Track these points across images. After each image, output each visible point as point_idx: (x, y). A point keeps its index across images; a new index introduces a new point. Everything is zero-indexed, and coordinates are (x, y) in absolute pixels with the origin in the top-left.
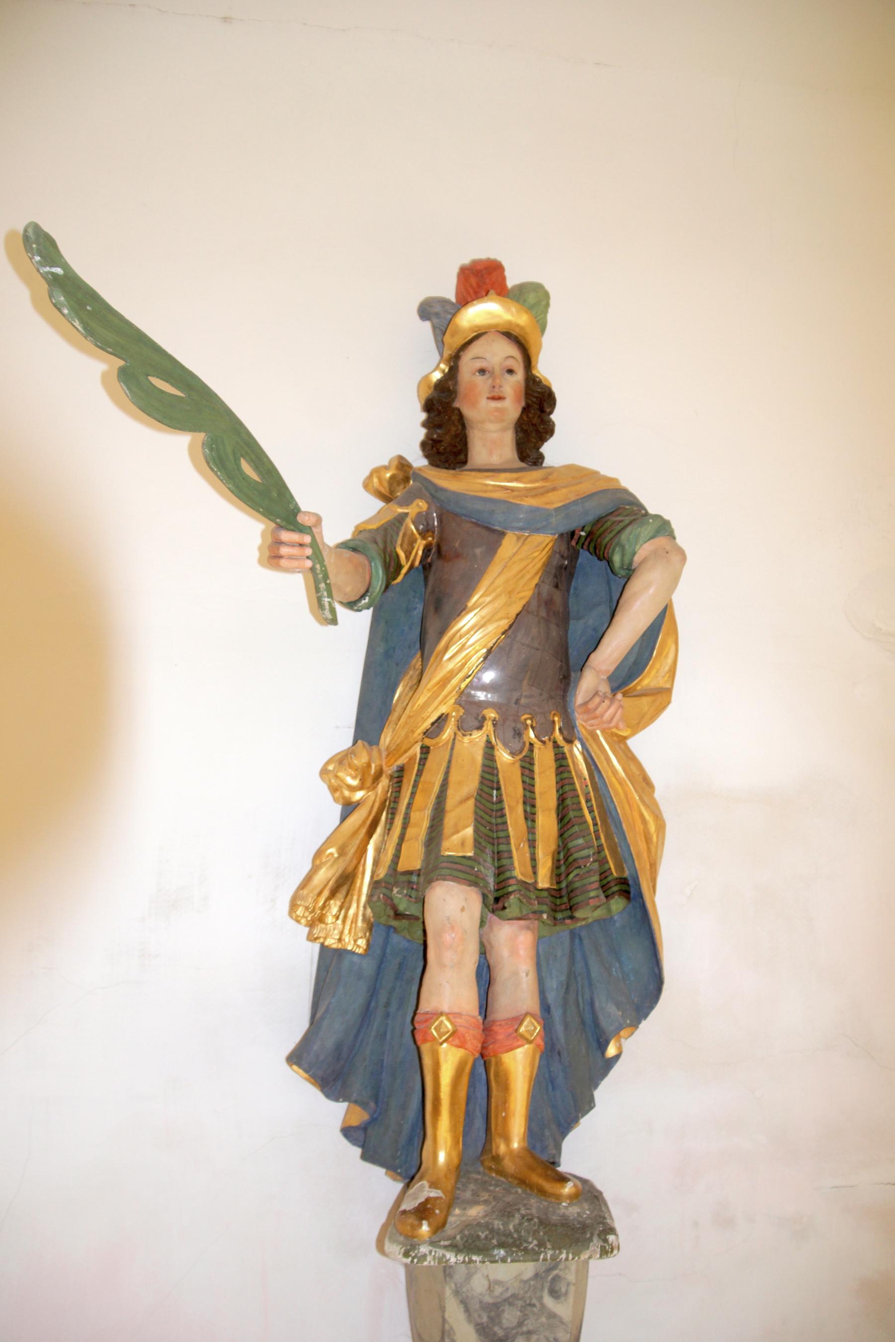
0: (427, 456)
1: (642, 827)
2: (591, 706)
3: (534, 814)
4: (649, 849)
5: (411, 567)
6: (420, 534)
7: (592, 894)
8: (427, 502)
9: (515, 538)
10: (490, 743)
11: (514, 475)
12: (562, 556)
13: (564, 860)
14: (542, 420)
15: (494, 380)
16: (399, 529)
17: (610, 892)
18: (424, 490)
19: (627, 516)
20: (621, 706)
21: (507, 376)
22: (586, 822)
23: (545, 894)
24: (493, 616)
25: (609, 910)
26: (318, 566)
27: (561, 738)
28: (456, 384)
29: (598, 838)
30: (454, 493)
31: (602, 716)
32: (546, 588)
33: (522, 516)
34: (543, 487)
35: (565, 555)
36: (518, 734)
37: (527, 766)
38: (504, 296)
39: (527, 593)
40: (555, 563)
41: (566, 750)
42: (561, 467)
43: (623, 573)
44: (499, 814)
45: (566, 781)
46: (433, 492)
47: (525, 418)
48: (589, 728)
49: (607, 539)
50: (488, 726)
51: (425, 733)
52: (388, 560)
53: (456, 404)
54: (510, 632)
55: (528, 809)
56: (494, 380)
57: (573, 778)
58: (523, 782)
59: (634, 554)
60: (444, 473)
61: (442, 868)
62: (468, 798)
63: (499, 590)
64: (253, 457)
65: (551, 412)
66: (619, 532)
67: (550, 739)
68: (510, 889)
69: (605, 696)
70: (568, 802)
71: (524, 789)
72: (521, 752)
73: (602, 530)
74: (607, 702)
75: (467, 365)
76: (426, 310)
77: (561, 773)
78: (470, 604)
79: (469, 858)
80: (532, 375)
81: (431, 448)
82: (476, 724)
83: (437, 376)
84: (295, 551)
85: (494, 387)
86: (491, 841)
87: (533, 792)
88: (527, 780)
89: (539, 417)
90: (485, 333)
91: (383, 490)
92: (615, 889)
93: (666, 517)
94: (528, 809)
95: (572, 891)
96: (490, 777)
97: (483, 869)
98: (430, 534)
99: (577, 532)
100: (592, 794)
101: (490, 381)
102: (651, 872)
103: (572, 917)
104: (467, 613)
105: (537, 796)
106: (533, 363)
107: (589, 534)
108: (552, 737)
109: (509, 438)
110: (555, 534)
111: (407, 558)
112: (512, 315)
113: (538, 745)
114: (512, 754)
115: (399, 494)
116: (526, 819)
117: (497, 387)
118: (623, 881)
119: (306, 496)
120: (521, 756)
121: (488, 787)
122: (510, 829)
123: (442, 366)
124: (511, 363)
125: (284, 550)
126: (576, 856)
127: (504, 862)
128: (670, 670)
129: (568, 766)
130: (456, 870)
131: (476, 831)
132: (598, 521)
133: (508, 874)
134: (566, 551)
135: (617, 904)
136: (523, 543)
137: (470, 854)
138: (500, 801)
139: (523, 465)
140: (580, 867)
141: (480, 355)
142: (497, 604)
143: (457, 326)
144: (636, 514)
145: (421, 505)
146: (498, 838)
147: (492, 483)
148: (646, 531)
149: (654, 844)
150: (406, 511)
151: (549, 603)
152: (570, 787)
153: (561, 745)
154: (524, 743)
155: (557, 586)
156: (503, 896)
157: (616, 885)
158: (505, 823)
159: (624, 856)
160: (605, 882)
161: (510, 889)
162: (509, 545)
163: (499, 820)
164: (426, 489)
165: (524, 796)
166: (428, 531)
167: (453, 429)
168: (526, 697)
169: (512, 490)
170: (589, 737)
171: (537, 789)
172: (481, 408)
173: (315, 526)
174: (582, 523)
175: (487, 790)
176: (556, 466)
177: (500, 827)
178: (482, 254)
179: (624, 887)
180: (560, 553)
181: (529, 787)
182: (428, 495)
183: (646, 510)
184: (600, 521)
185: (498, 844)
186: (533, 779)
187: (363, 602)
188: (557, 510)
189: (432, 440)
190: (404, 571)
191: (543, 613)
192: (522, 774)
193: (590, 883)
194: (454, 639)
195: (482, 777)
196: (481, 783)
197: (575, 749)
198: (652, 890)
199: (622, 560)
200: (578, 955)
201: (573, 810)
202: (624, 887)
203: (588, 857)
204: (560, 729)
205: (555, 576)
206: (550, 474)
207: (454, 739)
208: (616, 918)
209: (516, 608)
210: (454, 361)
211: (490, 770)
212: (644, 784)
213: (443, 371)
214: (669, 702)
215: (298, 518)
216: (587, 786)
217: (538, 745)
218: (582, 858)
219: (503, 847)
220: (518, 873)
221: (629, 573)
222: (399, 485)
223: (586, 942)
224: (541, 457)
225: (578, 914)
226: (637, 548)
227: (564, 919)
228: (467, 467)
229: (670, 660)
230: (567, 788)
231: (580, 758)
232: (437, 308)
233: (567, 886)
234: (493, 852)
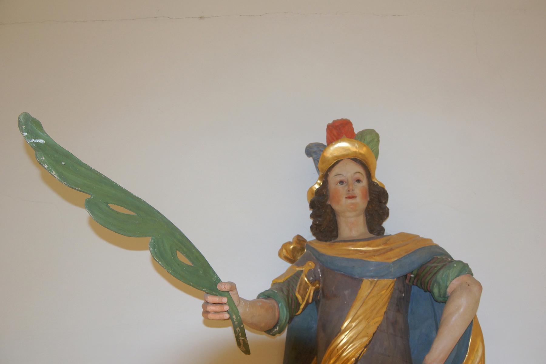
0: (314, 234)
5: (307, 304)
6: (311, 283)
9: (369, 282)
11: (366, 243)
12: (400, 291)
16: (297, 281)
19: (439, 262)
21: (357, 184)
24: (358, 336)
26: (234, 317)
28: (327, 190)
33: (372, 269)
34: (384, 249)
38: (351, 138)
39: (379, 319)
42: (396, 235)
47: (370, 207)
52: (290, 301)
54: (370, 346)
59: (447, 287)
60: (324, 244)
63: (360, 318)
64: (185, 250)
65: (386, 202)
66: (436, 273)
75: (333, 178)
80: (372, 181)
81: (315, 229)
83: (317, 187)
84: (217, 308)
85: (349, 191)
90: (342, 160)
91: (289, 257)
93: (465, 261)
98: (317, 282)
99: (408, 275)
101: (346, 188)
106: (372, 175)
107: (417, 276)
109: (361, 220)
111: (303, 299)
112: (356, 148)
115: (299, 258)
117: (351, 191)
119: (224, 273)
123: (319, 181)
124: (358, 176)
125: (211, 308)
128: (480, 360)
136: (374, 286)
139: (372, 235)
142: (360, 327)
143: (324, 157)
144: (446, 261)
145: (311, 265)
147: (353, 249)
150: (302, 269)
151: (394, 323)
155: (398, 311)
162: (366, 288)
166: (316, 280)
172: (345, 202)
173: (231, 290)
176: (393, 234)
178: (339, 117)
183: (451, 257)
184: (422, 267)
187: (275, 330)
188: (394, 263)
189: (316, 225)
190: (302, 307)
199: (439, 292)
206: (388, 240)
209: (372, 329)
210: (325, 178)
213: (320, 184)
215: (218, 287)
221: (444, 300)
222: (298, 252)
224: (383, 229)
226: (448, 283)
228: (338, 239)
229: (480, 353)
232: (315, 149)
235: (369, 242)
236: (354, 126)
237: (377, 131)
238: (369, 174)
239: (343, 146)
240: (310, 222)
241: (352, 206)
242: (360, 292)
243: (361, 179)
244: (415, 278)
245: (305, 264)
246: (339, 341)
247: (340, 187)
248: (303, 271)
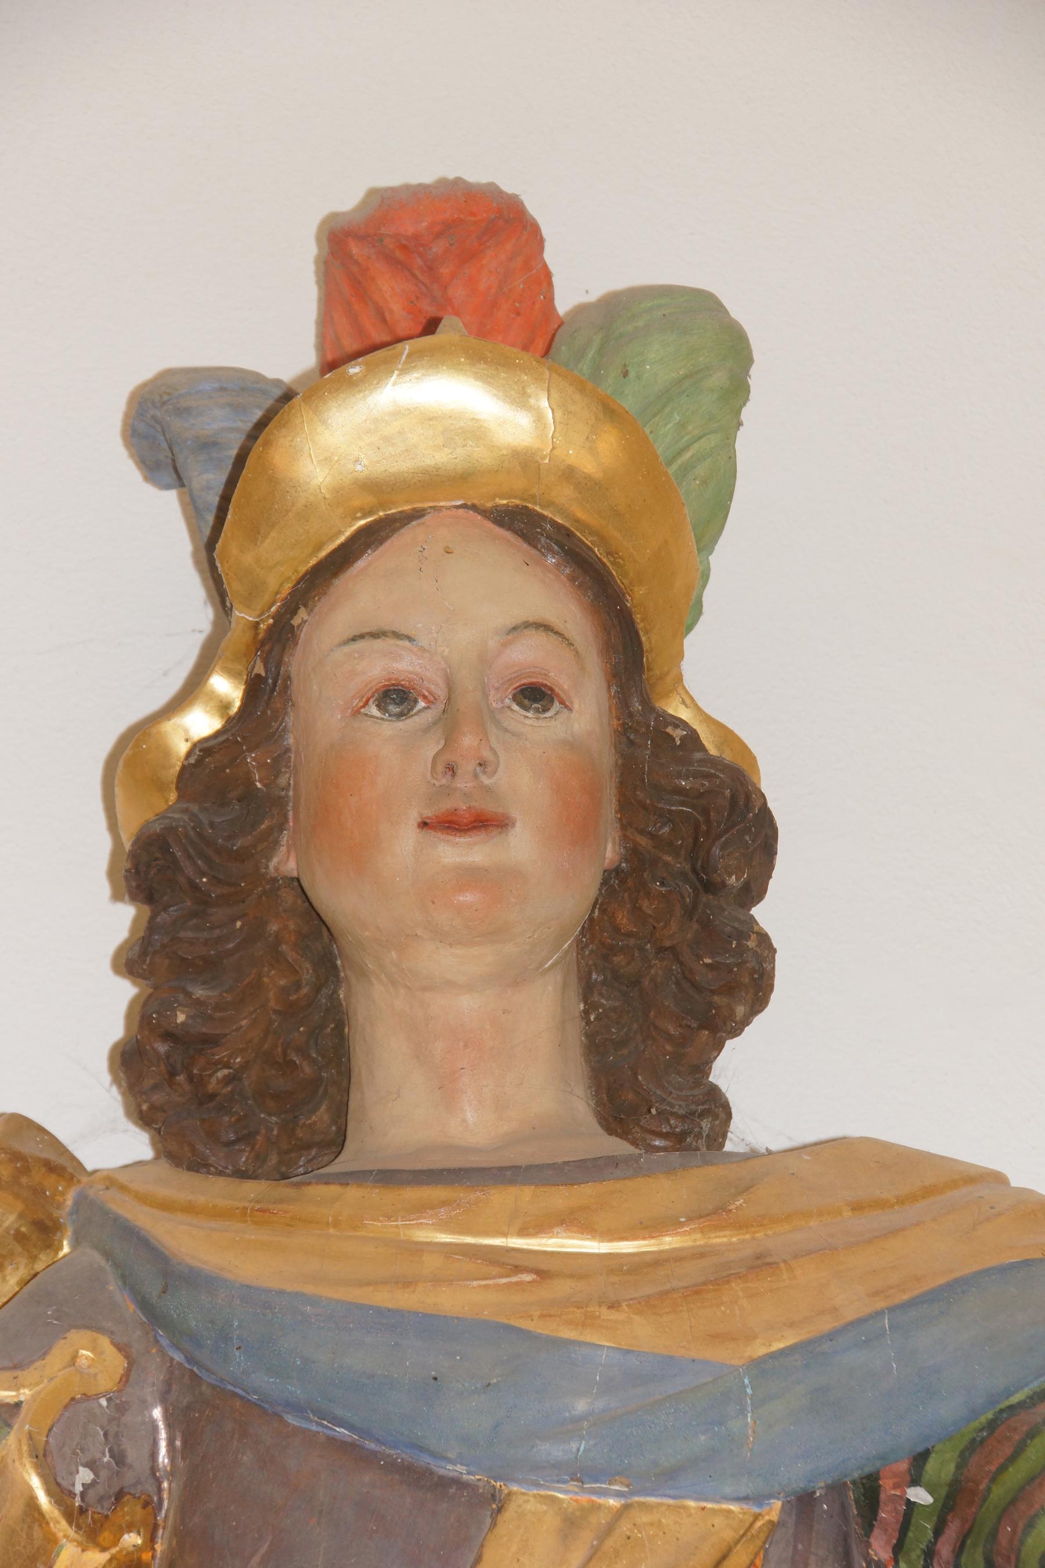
6: (73, 1515)
8: (121, 1348)
9: (552, 1521)
11: (560, 1198)
14: (706, 925)
15: (450, 739)
18: (112, 1285)
21: (525, 721)
28: (280, 761)
30: (249, 1293)
33: (581, 1406)
34: (700, 1254)
46: (152, 1289)
47: (623, 919)
53: (284, 862)
56: (450, 739)
65: (754, 891)
73: (1016, 1474)
75: (333, 666)
76: (161, 429)
81: (157, 1068)
85: (451, 769)
89: (690, 913)
90: (417, 514)
98: (132, 1510)
99: (887, 1488)
101: (431, 748)
107: (955, 1497)
110: (759, 1499)
117: (467, 767)
124: (530, 655)
132: (992, 1425)
141: (386, 620)
164: (126, 1279)
167: (275, 981)
169: (544, 1269)
174: (906, 1435)
182: (131, 1307)
210: (268, 652)
213: (223, 706)
224: (716, 1108)
228: (338, 1166)
235: (586, 1192)
236: (551, 256)
237: (736, 311)
238: (631, 646)
239: (445, 409)
240: (110, 1005)
241: (468, 898)
243: (560, 679)
247: (384, 732)
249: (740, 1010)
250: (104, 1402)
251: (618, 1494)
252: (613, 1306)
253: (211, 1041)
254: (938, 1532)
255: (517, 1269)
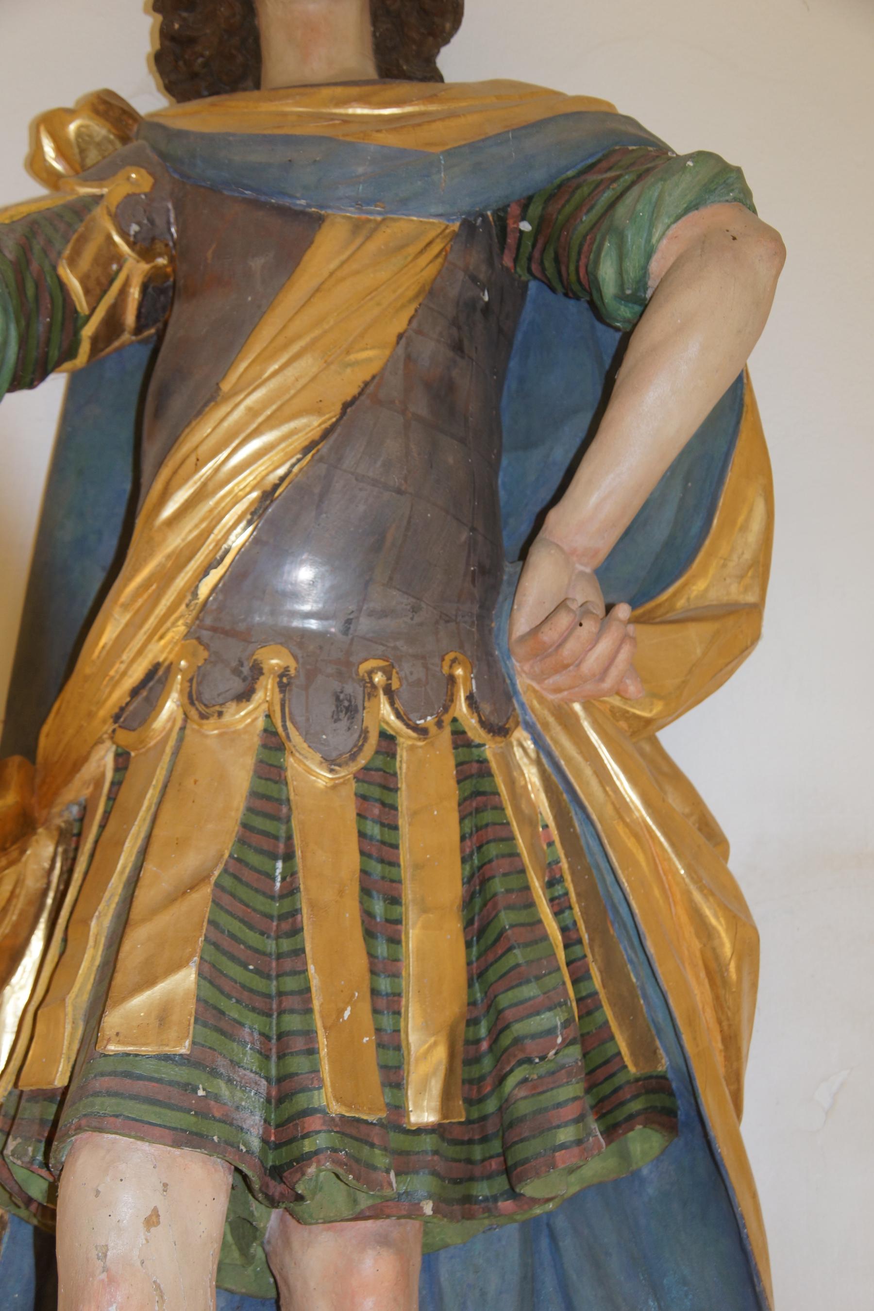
1: (696, 945)
2: (549, 635)
3: (398, 922)
4: (719, 1003)
7: (565, 1135)
8: (151, 174)
10: (275, 734)
12: (474, 279)
13: (482, 1052)
17: (621, 1115)
20: (625, 638)
22: (545, 937)
23: (428, 1142)
25: (625, 1156)
27: (474, 721)
29: (580, 977)
30: (202, 136)
31: (578, 662)
32: (431, 349)
33: (360, 170)
35: (482, 277)
36: (348, 709)
37: (377, 791)
39: (371, 358)
40: (453, 292)
41: (490, 750)
43: (625, 312)
44: (286, 926)
45: (491, 833)
48: (551, 697)
49: (582, 229)
50: (266, 692)
51: (116, 718)
52: (30, 291)
54: (324, 447)
55: (378, 907)
57: (508, 824)
58: (362, 835)
61: (96, 1094)
62: (194, 886)
66: (612, 205)
67: (439, 724)
68: (308, 1146)
69: (585, 610)
70: (498, 886)
71: (362, 853)
72: (353, 757)
74: (590, 626)
77: (478, 810)
78: (226, 386)
79: (184, 1060)
82: (237, 685)
86: (259, 1003)
87: (394, 864)
88: (374, 830)
92: (636, 1106)
93: (731, 159)
94: (378, 907)
95: (511, 1125)
96: (268, 825)
97: (224, 1090)
100: (565, 865)
102: (727, 1058)
103: (513, 1194)
104: (217, 405)
105: (406, 873)
107: (540, 226)
108: (447, 718)
113: (406, 738)
114: (331, 762)
116: (369, 934)
118: (655, 1085)
120: (354, 767)
121: (260, 851)
122: (311, 969)
126: (519, 1029)
127: (298, 1064)
129: (497, 793)
130: (135, 1097)
131: (209, 975)
132: (560, 186)
133: (301, 1101)
134: (483, 267)
135: (644, 1144)
137: (184, 1049)
138: (291, 891)
140: (529, 1061)
145: (137, 180)
146: (280, 994)
148: (677, 190)
149: (731, 991)
152: (502, 847)
153: (477, 741)
154: (364, 734)
156: (289, 1165)
157: (635, 1097)
158: (299, 952)
159: (657, 1024)
160: (607, 1088)
161: (308, 1146)
163: (286, 945)
165: (364, 872)
168: (371, 614)
170: (551, 720)
171: (405, 856)
175: (254, 859)
177: (288, 964)
179: (659, 1100)
180: (466, 270)
181: (379, 853)
185: (280, 1014)
186: (395, 828)
190: (88, 331)
191: (420, 406)
192: (361, 816)
193: (559, 1105)
194: (181, 472)
195: (245, 826)
196: (242, 841)
197: (518, 752)
198: (731, 1106)
199: (621, 272)
200: (549, 1283)
201: (509, 907)
202: (659, 1100)
203: (551, 1032)
204: (470, 698)
205: (455, 323)
207: (183, 729)
208: (645, 1172)
209: (345, 384)
211: (268, 807)
212: (701, 839)
214: (756, 637)
216: (551, 844)
217: (406, 738)
218: (533, 1036)
219: (293, 1022)
220: (328, 1099)
223: (567, 1243)
225: (529, 1189)
227: (495, 1199)
230: (493, 850)
231: (531, 776)
233: (500, 1109)
234: (266, 1037)
242: (306, 258)
244: (538, 231)
245: (114, 174)
246: (596, 949)
248: (101, 197)
249: (448, 26)
250: (143, 197)
251: (379, 213)
252: (379, 131)
253: (192, 41)
254: (534, 246)
255: (332, 119)
